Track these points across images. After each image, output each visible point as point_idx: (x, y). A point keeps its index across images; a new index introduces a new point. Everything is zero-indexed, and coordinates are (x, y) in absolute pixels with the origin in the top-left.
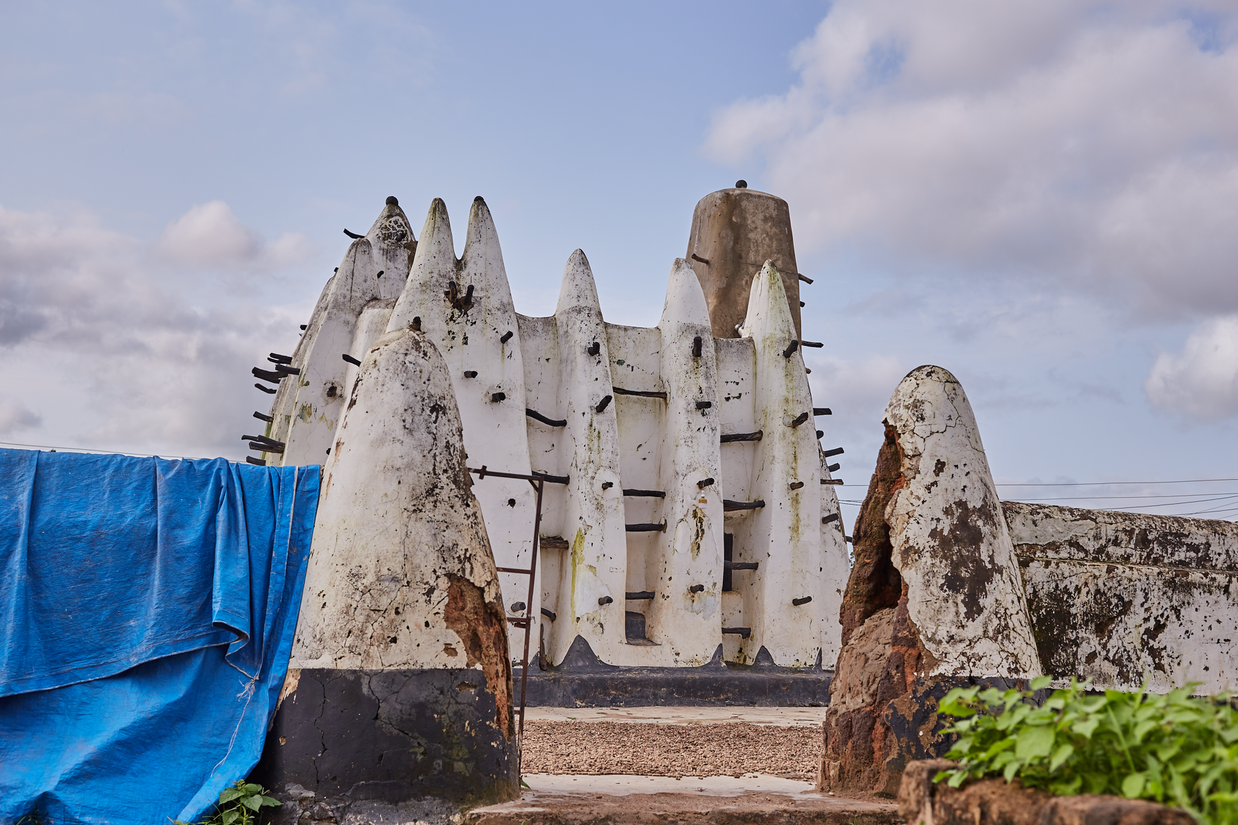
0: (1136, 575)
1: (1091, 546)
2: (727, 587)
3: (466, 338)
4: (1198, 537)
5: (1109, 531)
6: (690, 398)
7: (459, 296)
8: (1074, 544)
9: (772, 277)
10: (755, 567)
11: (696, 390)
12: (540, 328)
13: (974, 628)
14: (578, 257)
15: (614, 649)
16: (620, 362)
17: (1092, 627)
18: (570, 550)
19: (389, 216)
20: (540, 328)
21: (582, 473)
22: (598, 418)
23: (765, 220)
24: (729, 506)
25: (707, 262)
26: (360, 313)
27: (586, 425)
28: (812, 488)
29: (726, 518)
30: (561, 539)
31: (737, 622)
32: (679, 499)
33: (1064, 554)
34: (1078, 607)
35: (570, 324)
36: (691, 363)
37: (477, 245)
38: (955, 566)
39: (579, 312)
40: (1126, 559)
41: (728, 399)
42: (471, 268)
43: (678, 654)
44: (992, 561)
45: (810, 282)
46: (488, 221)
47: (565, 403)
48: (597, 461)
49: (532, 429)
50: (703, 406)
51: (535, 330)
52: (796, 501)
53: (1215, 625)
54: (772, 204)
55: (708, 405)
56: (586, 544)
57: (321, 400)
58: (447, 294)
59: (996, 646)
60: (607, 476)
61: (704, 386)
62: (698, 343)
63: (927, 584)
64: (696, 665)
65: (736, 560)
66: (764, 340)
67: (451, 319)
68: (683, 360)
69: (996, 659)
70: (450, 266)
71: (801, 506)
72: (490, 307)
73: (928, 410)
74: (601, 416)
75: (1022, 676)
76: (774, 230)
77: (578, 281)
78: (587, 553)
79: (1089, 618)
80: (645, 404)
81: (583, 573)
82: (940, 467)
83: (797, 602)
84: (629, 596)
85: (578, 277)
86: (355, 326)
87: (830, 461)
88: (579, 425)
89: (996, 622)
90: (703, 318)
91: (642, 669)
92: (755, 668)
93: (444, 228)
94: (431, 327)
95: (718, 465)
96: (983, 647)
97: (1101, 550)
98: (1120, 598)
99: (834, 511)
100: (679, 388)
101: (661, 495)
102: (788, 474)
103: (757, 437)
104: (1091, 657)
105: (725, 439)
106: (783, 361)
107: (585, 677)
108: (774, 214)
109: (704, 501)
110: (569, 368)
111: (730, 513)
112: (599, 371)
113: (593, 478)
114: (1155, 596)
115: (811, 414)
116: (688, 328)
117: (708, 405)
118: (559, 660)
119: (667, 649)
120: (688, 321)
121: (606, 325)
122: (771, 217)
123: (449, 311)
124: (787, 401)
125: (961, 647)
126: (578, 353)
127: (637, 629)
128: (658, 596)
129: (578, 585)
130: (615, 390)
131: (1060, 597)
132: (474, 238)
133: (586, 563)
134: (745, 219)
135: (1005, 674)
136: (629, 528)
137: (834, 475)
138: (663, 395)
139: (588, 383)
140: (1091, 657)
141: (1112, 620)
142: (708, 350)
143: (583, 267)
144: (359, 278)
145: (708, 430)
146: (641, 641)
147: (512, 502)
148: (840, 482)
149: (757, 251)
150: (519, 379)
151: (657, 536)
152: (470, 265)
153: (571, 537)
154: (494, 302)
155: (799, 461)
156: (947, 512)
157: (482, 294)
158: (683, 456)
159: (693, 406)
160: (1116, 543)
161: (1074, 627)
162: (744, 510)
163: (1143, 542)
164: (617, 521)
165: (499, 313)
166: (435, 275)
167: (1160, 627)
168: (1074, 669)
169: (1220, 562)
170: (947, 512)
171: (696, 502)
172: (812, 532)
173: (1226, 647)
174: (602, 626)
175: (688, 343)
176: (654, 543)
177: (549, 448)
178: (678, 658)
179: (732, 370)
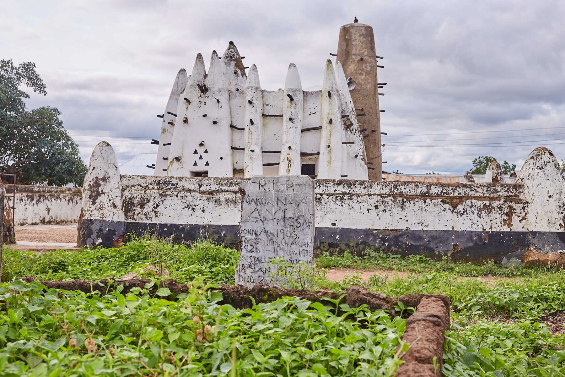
0: (152, 193)
1: (144, 185)
4: (174, 182)
11: (290, 113)
13: (93, 208)
16: (267, 105)
19: (229, 49)
23: (360, 36)
33: (136, 188)
34: (136, 202)
38: (92, 193)
40: (153, 188)
41: (310, 114)
44: (102, 191)
48: (251, 142)
52: (330, 151)
53: (173, 205)
54: (363, 29)
59: (98, 212)
69: (97, 215)
70: (202, 77)
75: (104, 219)
76: (364, 39)
82: (94, 168)
89: (99, 206)
97: (146, 186)
98: (147, 199)
102: (327, 142)
108: (364, 32)
111: (303, 157)
114: (156, 198)
120: (290, 87)
123: (199, 94)
124: (329, 114)
125: (89, 212)
134: (351, 36)
135: (99, 218)
136: (264, 165)
144: (180, 83)
147: (221, 158)
149: (356, 49)
152: (209, 76)
157: (212, 86)
158: (285, 138)
160: (151, 184)
163: (159, 183)
167: (158, 206)
169: (180, 188)
170: (93, 180)
173: (176, 211)
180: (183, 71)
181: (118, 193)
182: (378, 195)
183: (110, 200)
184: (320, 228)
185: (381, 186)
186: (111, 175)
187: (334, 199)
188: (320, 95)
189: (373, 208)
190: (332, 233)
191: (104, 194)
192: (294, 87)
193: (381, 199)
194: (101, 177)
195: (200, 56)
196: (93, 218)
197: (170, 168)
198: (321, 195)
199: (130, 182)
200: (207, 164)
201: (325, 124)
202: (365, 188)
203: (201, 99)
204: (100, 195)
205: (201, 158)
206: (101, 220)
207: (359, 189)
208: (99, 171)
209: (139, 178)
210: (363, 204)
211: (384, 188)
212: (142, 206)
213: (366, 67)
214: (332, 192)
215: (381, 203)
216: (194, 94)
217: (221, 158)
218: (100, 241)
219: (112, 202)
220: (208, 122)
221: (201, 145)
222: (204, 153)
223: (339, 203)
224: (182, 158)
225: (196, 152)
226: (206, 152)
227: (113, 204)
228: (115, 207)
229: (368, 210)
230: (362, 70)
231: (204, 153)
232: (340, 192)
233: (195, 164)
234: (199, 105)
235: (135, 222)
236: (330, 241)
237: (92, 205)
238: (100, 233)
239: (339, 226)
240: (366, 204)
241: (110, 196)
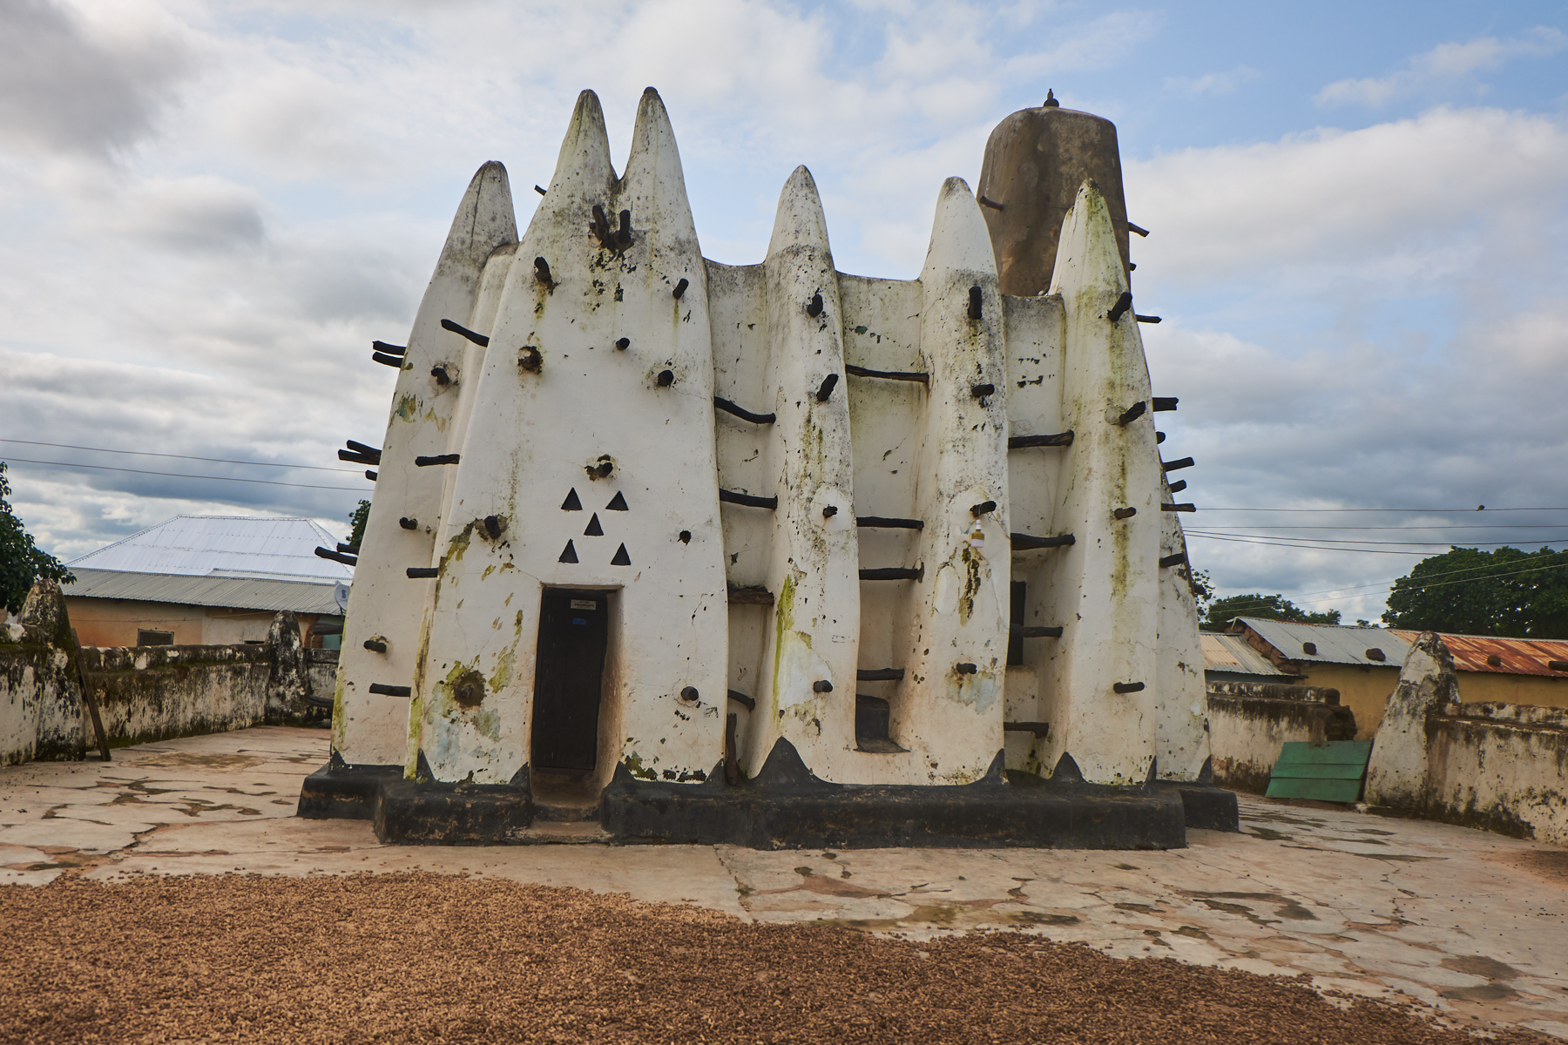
2: (1016, 658)
3: (619, 292)
6: (962, 380)
7: (612, 230)
9: (1092, 201)
10: (1057, 633)
11: (971, 368)
12: (740, 280)
14: (800, 177)
15: (835, 759)
16: (861, 330)
18: (776, 609)
20: (740, 280)
21: (794, 492)
22: (820, 410)
23: (1084, 147)
24: (1018, 542)
25: (1000, 208)
26: (484, 265)
27: (802, 421)
28: (1149, 518)
29: (1014, 560)
30: (764, 589)
31: (1028, 714)
32: (942, 532)
35: (783, 272)
36: (966, 328)
37: (642, 156)
39: (797, 253)
41: (1022, 384)
42: (633, 190)
43: (934, 765)
45: (1144, 233)
46: (661, 122)
47: (774, 389)
48: (816, 475)
49: (724, 429)
50: (981, 392)
51: (732, 283)
52: (1123, 536)
54: (1093, 126)
55: (990, 389)
56: (797, 600)
57: (429, 389)
58: (592, 226)
60: (829, 497)
61: (984, 362)
62: (976, 298)
64: (962, 782)
65: (1031, 622)
66: (1079, 297)
67: (599, 263)
68: (953, 324)
70: (601, 187)
71: (1130, 543)
72: (659, 246)
74: (823, 408)
76: (1096, 161)
77: (797, 210)
78: (800, 614)
80: (896, 391)
81: (791, 644)
83: (1120, 689)
84: (862, 675)
85: (798, 204)
86: (477, 283)
87: (1173, 476)
88: (791, 423)
90: (983, 259)
91: (878, 788)
92: (1054, 785)
93: (594, 131)
94: (567, 275)
95: (1003, 482)
99: (1178, 550)
100: (946, 365)
101: (917, 525)
102: (1111, 495)
103: (1065, 440)
105: (1018, 444)
106: (1107, 328)
107: (787, 802)
108: (1097, 139)
109: (979, 536)
110: (780, 336)
111: (1022, 553)
112: (822, 340)
113: (810, 500)
115: (1150, 406)
116: (963, 276)
117: (990, 389)
118: (757, 770)
119: (918, 758)
120: (962, 266)
121: (840, 276)
122: (1092, 143)
123: (595, 252)
124: (1112, 385)
126: (793, 314)
127: (875, 724)
128: (908, 676)
129: (784, 662)
130: (849, 369)
132: (640, 148)
133: (796, 628)
134: (1056, 146)
136: (864, 575)
137: (1179, 498)
138: (924, 378)
139: (804, 357)
142: (993, 309)
143: (806, 190)
144: (484, 216)
145: (989, 429)
146: (880, 744)
147: (685, 536)
148: (1190, 508)
150: (702, 351)
151: (909, 588)
152: (632, 185)
153: (777, 588)
154: (665, 238)
155: (1129, 477)
157: (646, 227)
158: (950, 467)
159: (967, 392)
162: (1041, 554)
164: (843, 571)
165: (672, 254)
166: (577, 200)
167: (37, 696)
171: (968, 537)
172: (1147, 583)
174: (817, 723)
175: (962, 299)
176: (905, 596)
177: (750, 455)
178: (935, 772)
179: (1031, 340)
180: (493, 172)
188: (1057, 315)
195: (589, 104)
197: (452, 564)
200: (622, 558)
201: (1095, 424)
203: (604, 277)
205: (594, 528)
216: (574, 260)
217: (685, 536)
220: (627, 378)
221: (603, 470)
222: (611, 506)
224: (512, 525)
225: (572, 502)
226: (618, 503)
231: (611, 506)
233: (569, 555)
234: (592, 298)
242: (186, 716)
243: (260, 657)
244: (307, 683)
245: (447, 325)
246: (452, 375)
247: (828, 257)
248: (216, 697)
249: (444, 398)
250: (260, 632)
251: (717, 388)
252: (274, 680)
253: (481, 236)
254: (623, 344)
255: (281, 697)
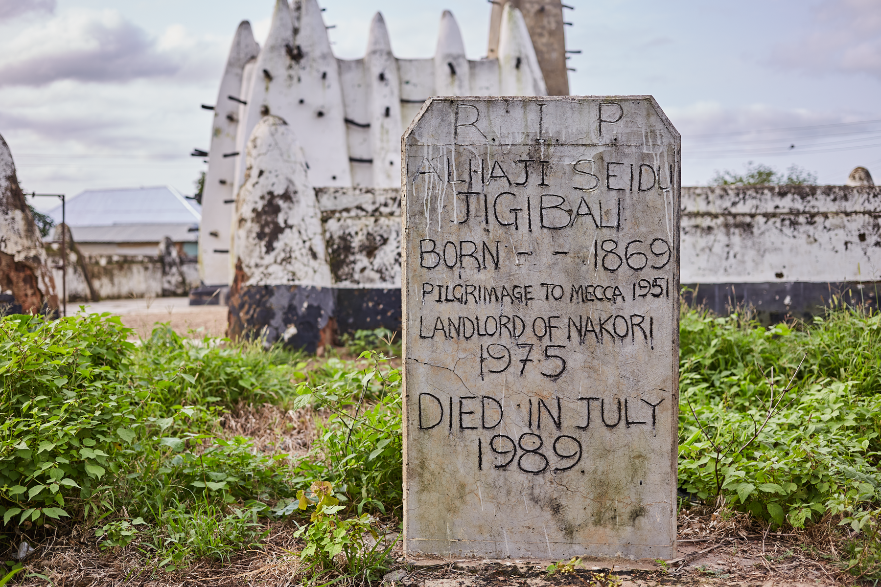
1: (370, 208)
5: (381, 199)
8: (359, 208)
13: (269, 259)
16: (407, 83)
17: (364, 253)
34: (356, 243)
38: (262, 227)
40: (392, 214)
44: (286, 222)
63: (248, 237)
69: (281, 274)
73: (259, 142)
75: (297, 283)
79: (362, 248)
82: (261, 173)
89: (283, 255)
96: (274, 269)
97: (376, 210)
98: (382, 236)
104: (363, 270)
121: (397, 60)
125: (261, 269)
131: (345, 239)
135: (285, 282)
140: (363, 270)
141: (376, 248)
144: (243, 45)
156: (262, 198)
160: (386, 205)
161: (353, 254)
168: (352, 275)
170: (262, 198)
181: (315, 225)
182: (864, 213)
183: (304, 242)
184: (753, 284)
185: (866, 196)
186: (299, 187)
187: (778, 224)
189: (856, 239)
190: (777, 293)
191: (291, 227)
192: (455, 51)
193: (871, 220)
194: (279, 190)
196: (272, 282)
198: (753, 216)
199: (337, 202)
202: (835, 200)
203: (292, 72)
204: (281, 230)
206: (291, 287)
207: (822, 204)
208: (274, 180)
209: (357, 192)
210: (836, 231)
211: (872, 200)
212: (370, 250)
213: (549, 23)
214: (770, 209)
215: (870, 228)
216: (280, 65)
218: (292, 330)
219: (308, 244)
220: (307, 114)
223: (788, 231)
227: (311, 249)
228: (314, 256)
229: (846, 243)
230: (543, 28)
232: (786, 210)
235: (355, 286)
236: (774, 309)
237: (267, 252)
238: (290, 315)
239: (790, 277)
240: (841, 232)
241: (303, 231)
242: (124, 290)
243: (156, 261)
244: (181, 274)
245: (231, 98)
246: (235, 117)
247: (389, 53)
248: (137, 280)
249: (233, 125)
250: (155, 252)
251: (345, 112)
252: (165, 273)
253: (243, 54)
254: (302, 102)
255: (169, 282)
